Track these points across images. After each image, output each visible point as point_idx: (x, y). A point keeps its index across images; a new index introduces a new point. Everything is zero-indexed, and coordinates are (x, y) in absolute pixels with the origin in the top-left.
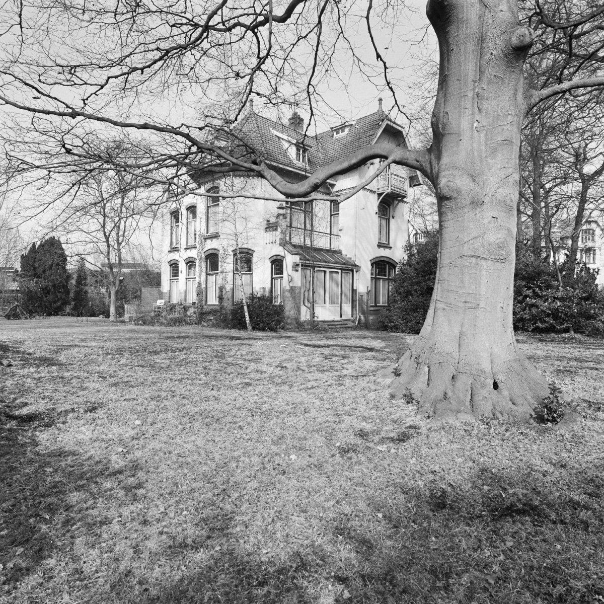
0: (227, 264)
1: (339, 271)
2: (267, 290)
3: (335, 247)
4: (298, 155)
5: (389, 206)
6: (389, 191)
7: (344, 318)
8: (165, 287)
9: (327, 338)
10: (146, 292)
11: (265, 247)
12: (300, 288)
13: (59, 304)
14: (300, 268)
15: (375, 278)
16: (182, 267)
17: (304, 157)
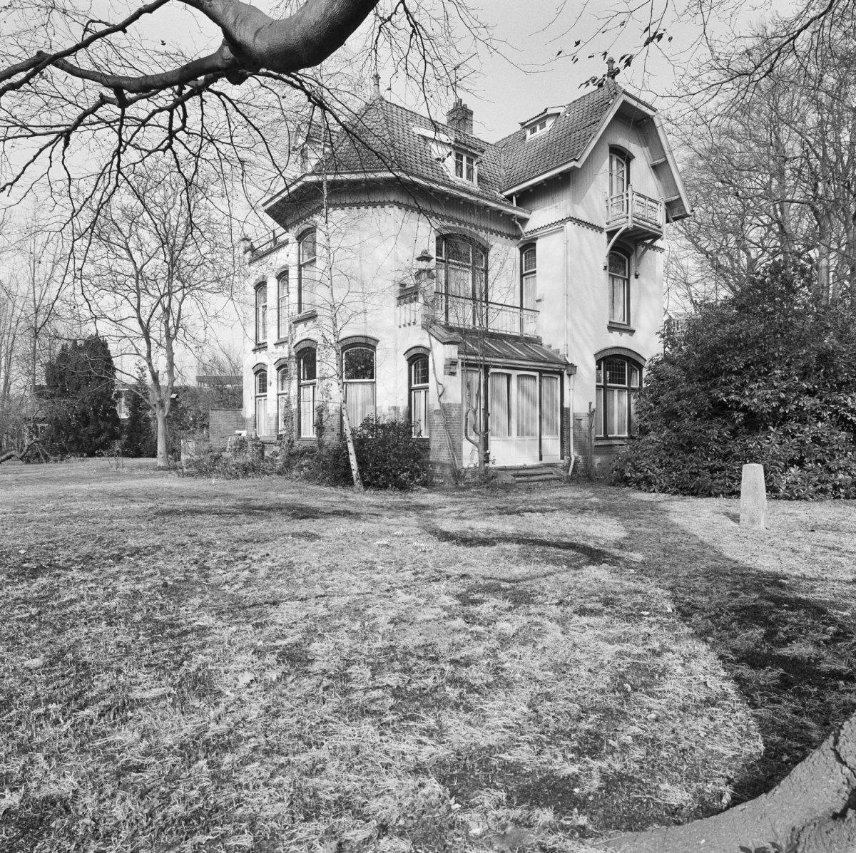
0: (328, 364)
1: (536, 374)
2: (401, 411)
3: (529, 330)
4: (458, 165)
5: (629, 256)
6: (630, 225)
7: (545, 460)
8: (248, 411)
9: (504, 511)
10: (218, 418)
11: (395, 331)
12: (460, 407)
13: (102, 438)
14: (458, 370)
15: (605, 388)
16: (272, 374)
17: (470, 170)
